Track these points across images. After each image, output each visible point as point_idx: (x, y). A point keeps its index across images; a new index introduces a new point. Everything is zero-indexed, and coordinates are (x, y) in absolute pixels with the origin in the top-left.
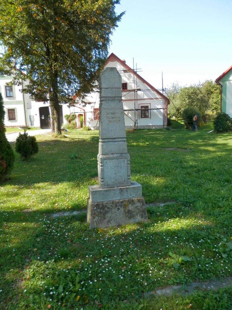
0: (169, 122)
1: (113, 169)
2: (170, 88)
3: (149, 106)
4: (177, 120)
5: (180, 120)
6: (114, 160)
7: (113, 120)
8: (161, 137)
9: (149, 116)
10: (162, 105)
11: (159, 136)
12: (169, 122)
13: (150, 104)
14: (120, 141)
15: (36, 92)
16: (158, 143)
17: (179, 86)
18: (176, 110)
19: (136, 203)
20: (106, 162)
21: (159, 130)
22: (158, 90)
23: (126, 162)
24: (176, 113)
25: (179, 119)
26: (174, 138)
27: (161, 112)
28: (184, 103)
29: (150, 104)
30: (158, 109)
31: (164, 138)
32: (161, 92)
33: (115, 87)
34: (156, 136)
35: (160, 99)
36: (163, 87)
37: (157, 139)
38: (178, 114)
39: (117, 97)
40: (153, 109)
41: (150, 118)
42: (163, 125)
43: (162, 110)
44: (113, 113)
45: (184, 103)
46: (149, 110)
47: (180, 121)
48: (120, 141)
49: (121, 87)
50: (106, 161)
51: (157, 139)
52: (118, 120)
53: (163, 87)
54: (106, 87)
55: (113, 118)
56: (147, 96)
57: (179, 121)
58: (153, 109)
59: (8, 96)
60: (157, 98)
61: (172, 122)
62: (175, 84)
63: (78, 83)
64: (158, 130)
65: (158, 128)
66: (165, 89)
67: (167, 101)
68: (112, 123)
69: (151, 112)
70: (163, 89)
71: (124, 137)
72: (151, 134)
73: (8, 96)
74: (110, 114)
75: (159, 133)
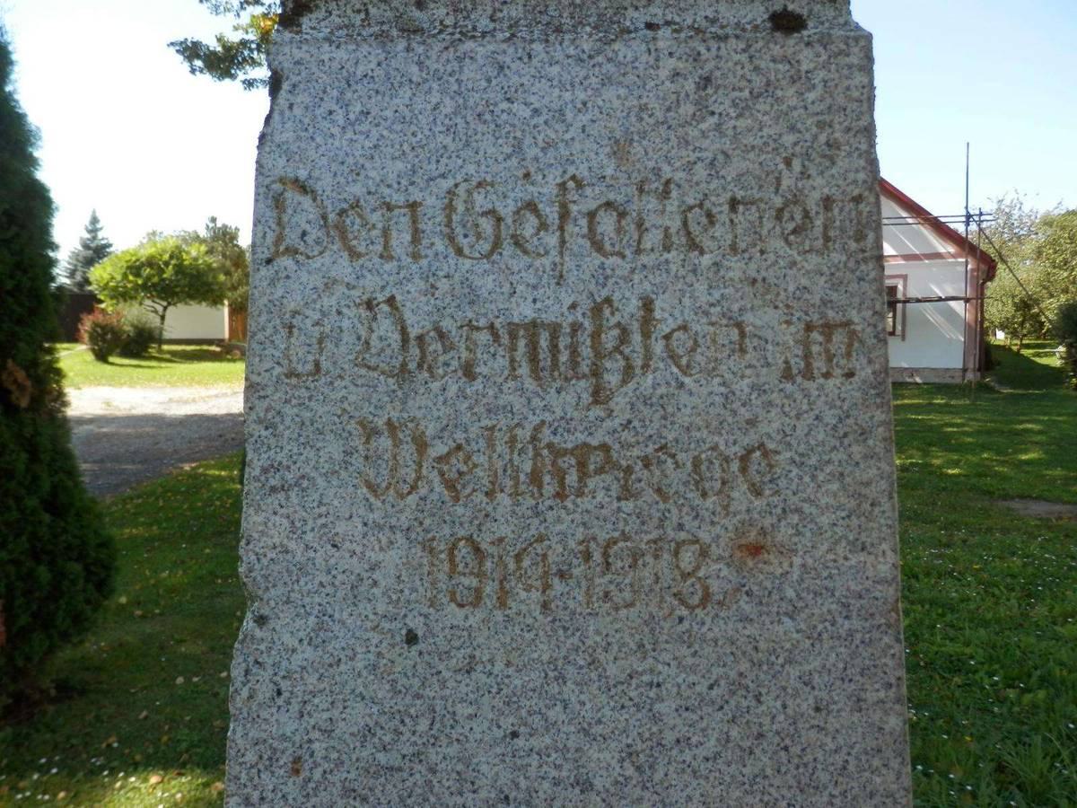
0: (988, 358)
3: (900, 287)
4: (1015, 348)
5: (1028, 346)
8: (963, 425)
9: (899, 328)
10: (964, 285)
11: (947, 418)
12: (988, 358)
13: (905, 277)
16: (956, 464)
17: (1026, 209)
18: (1015, 304)
21: (941, 387)
22: (943, 220)
24: (1014, 317)
25: (1024, 342)
26: (1039, 438)
27: (952, 312)
28: (1066, 274)
29: (905, 277)
30: (940, 299)
31: (979, 432)
32: (961, 228)
34: (934, 418)
35: (953, 256)
36: (967, 208)
37: (945, 442)
38: (1022, 324)
40: (918, 301)
41: (903, 337)
42: (965, 370)
43: (958, 306)
45: (1066, 274)
46: (899, 306)
47: (1031, 351)
51: (945, 442)
52: (717, 534)
53: (967, 208)
56: (894, 248)
57: (1026, 352)
58: (918, 301)
60: (938, 256)
61: (995, 355)
62: (1007, 202)
64: (940, 389)
65: (937, 380)
66: (981, 214)
67: (986, 265)
68: (527, 599)
69: (908, 311)
70: (969, 216)
72: (911, 405)
74: (493, 365)
75: (946, 405)
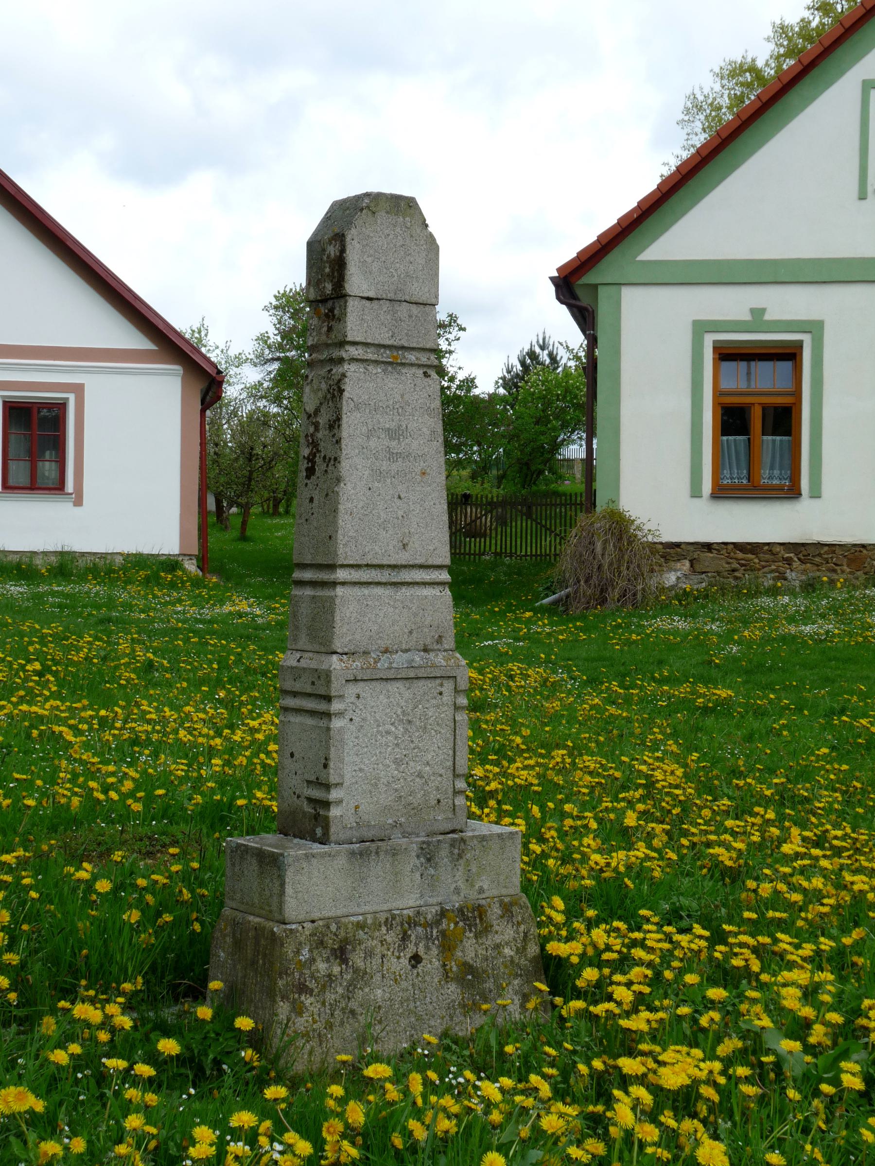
1: (388, 733)
2: (807, 14)
6: (393, 687)
7: (394, 467)
14: (425, 584)
15: (222, 745)
19: (496, 928)
20: (358, 697)
23: (447, 698)
33: (407, 298)
39: (413, 349)
44: (394, 434)
48: (425, 584)
49: (351, 690)
50: (359, 688)
52: (418, 470)
54: (371, 294)
55: (393, 456)
59: (11, 483)
63: (299, 979)
71: (438, 562)
73: (11, 483)
